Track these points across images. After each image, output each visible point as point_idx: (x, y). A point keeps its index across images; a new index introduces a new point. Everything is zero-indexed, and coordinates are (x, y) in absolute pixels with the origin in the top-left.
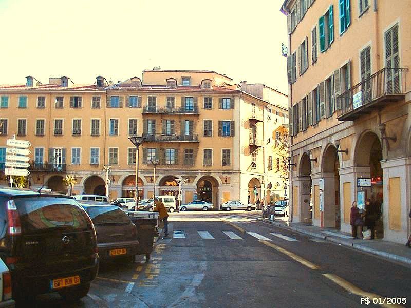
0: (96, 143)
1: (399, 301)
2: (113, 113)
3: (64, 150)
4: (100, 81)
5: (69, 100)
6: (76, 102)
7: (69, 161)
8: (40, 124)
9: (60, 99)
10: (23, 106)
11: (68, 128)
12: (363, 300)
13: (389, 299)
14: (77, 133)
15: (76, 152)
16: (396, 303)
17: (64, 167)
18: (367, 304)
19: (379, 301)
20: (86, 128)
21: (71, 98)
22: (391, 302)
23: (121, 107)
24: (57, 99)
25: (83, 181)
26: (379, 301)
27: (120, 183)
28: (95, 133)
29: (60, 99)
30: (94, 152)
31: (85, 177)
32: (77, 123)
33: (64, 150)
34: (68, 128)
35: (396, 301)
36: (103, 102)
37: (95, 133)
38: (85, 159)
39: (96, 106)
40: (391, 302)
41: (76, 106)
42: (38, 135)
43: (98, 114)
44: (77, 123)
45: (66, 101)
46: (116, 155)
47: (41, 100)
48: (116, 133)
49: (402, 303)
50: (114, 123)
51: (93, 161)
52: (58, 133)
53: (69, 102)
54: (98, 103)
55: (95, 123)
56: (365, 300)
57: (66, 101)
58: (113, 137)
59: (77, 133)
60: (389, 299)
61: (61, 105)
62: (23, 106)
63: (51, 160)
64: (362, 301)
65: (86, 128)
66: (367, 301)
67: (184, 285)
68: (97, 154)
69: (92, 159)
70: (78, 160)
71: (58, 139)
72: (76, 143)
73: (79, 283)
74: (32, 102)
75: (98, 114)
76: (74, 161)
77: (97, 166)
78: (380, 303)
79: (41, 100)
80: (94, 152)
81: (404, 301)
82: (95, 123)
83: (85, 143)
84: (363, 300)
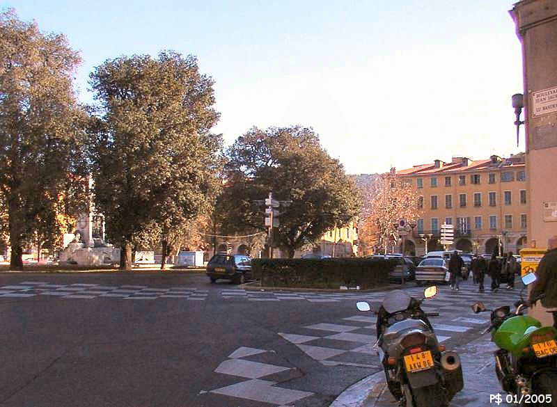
0: (494, 212)
1: (541, 399)
2: (507, 186)
3: (468, 219)
4: (393, 170)
5: (470, 177)
6: (476, 180)
7: (473, 227)
8: (448, 198)
9: (463, 178)
10: (434, 185)
11: (470, 201)
12: (492, 397)
13: (528, 397)
14: (478, 205)
15: (478, 220)
16: (538, 401)
17: (469, 231)
18: (498, 402)
19: (514, 398)
20: (485, 200)
21: (472, 177)
22: (530, 400)
23: (513, 180)
24: (461, 177)
25: (485, 242)
26: (514, 398)
27: (515, 243)
28: (493, 204)
29: (463, 178)
30: (493, 219)
31: (486, 240)
32: (477, 196)
33: (468, 219)
34: (470, 201)
35: (538, 398)
36: (497, 178)
37: (493, 204)
38: (486, 225)
39: (492, 181)
40: (530, 400)
41: (476, 183)
42: (447, 208)
43: (494, 188)
44: (477, 196)
45: (468, 179)
46: (510, 221)
47: (448, 179)
48: (510, 203)
49: (545, 401)
50: (508, 195)
51: (491, 227)
52: (463, 205)
53: (469, 180)
54: (494, 179)
55: (492, 195)
56: (495, 397)
57: (468, 179)
58: (508, 207)
59: (478, 205)
60: (528, 397)
61: (464, 182)
62: (434, 185)
63: (459, 227)
64: (491, 399)
65: (485, 200)
66: (498, 399)
67: (456, 360)
68: (495, 220)
69: (491, 225)
70: (480, 225)
71: (462, 210)
72: (478, 213)
73: (429, 352)
74: (441, 182)
75: (494, 188)
76: (476, 227)
77: (495, 230)
78: (516, 402)
79: (448, 179)
80: (493, 219)
81: (548, 400)
82: (492, 195)
83: (485, 212)
84: (492, 397)
